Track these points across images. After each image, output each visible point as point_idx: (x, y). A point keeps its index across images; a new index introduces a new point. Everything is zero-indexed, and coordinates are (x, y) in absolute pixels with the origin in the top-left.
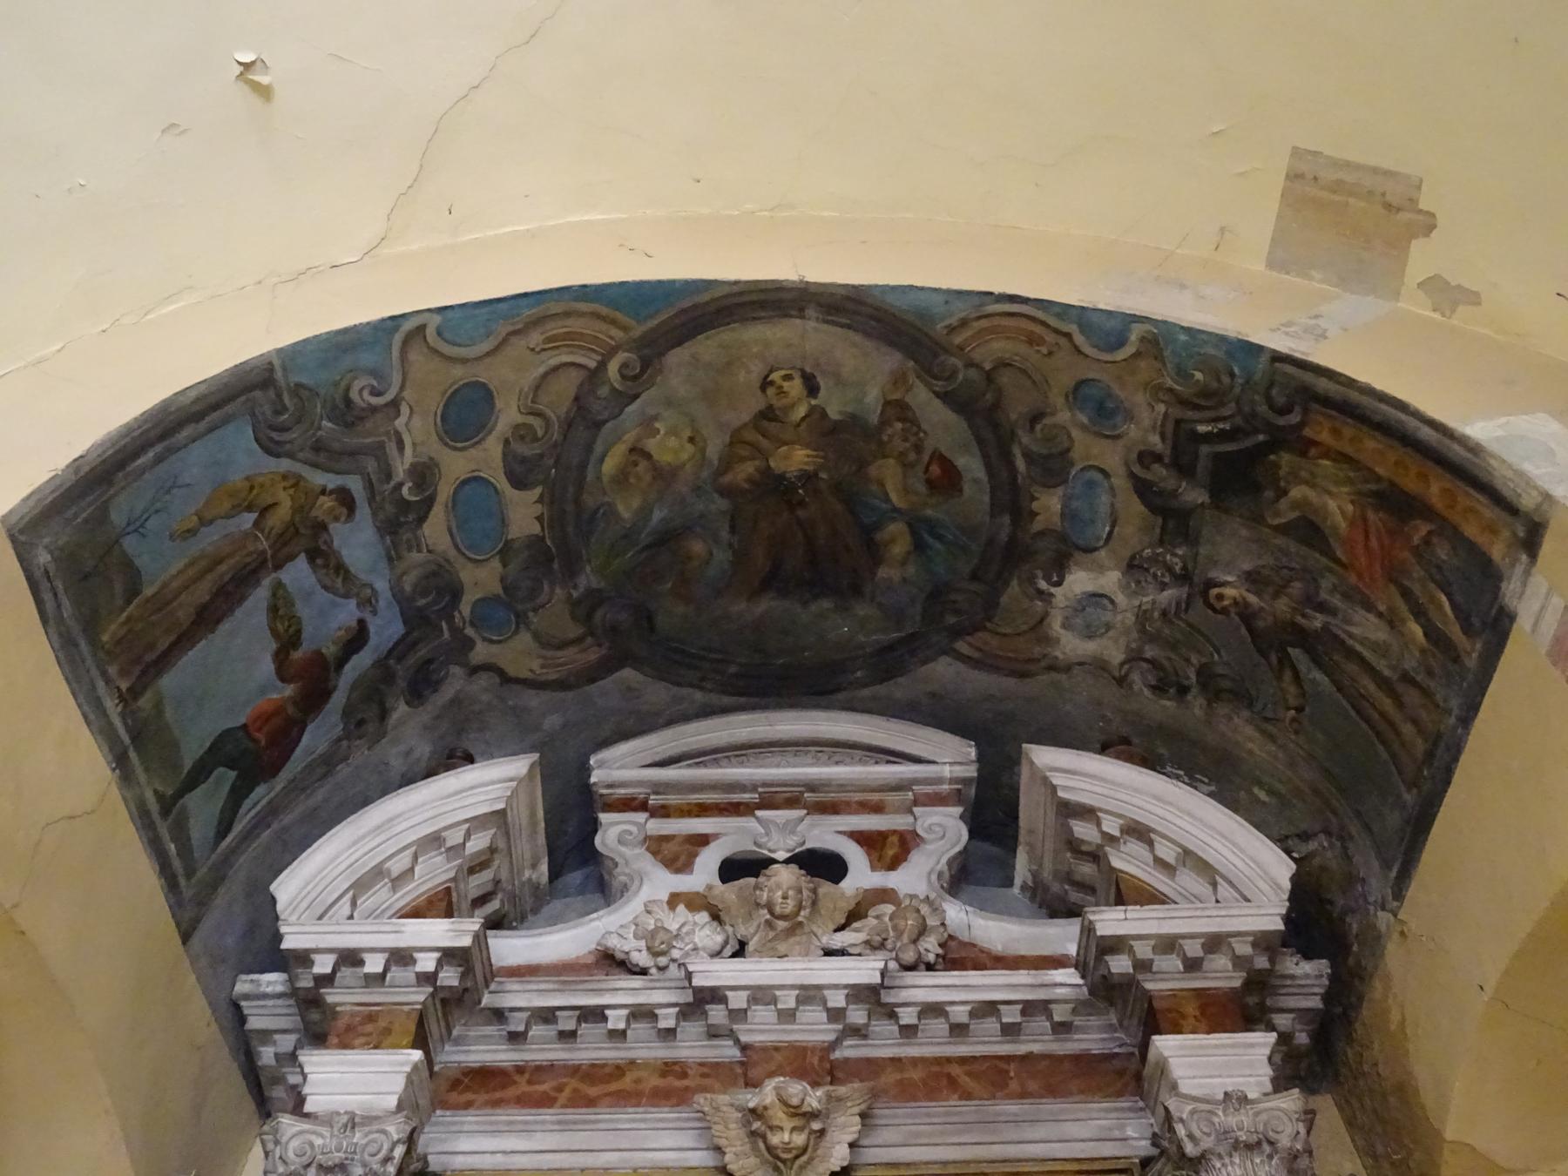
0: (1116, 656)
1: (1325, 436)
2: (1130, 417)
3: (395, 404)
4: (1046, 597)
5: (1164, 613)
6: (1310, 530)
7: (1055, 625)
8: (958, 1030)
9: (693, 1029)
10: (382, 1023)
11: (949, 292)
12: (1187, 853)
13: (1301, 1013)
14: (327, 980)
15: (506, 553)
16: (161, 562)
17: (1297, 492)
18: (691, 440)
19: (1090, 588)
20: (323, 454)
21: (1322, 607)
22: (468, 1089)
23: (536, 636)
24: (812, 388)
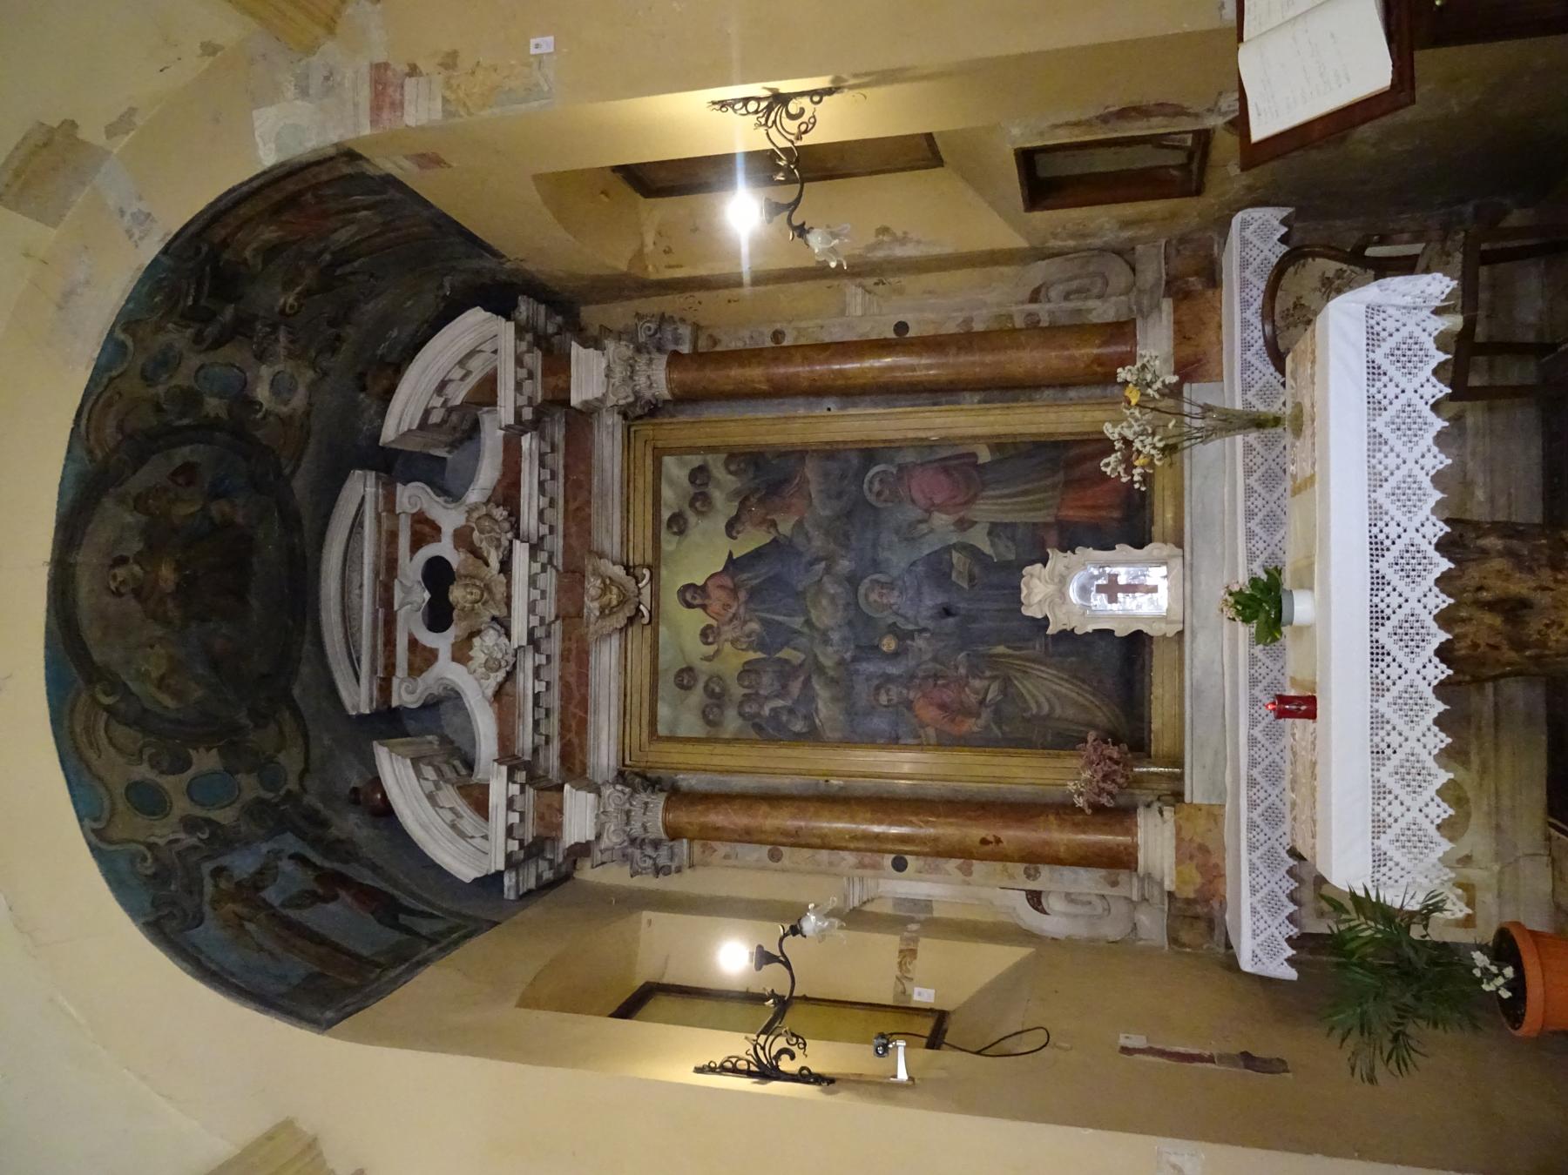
0: (310, 374)
1: (223, 233)
2: (170, 346)
3: (151, 846)
4: (268, 413)
5: (292, 342)
6: (271, 252)
7: (284, 410)
8: (552, 503)
9: (544, 646)
11: (67, 459)
13: (548, 317)
14: (521, 842)
15: (231, 771)
16: (298, 967)
17: (248, 254)
18: (152, 647)
19: (267, 387)
20: (193, 887)
21: (321, 253)
23: (278, 751)
24: (122, 561)
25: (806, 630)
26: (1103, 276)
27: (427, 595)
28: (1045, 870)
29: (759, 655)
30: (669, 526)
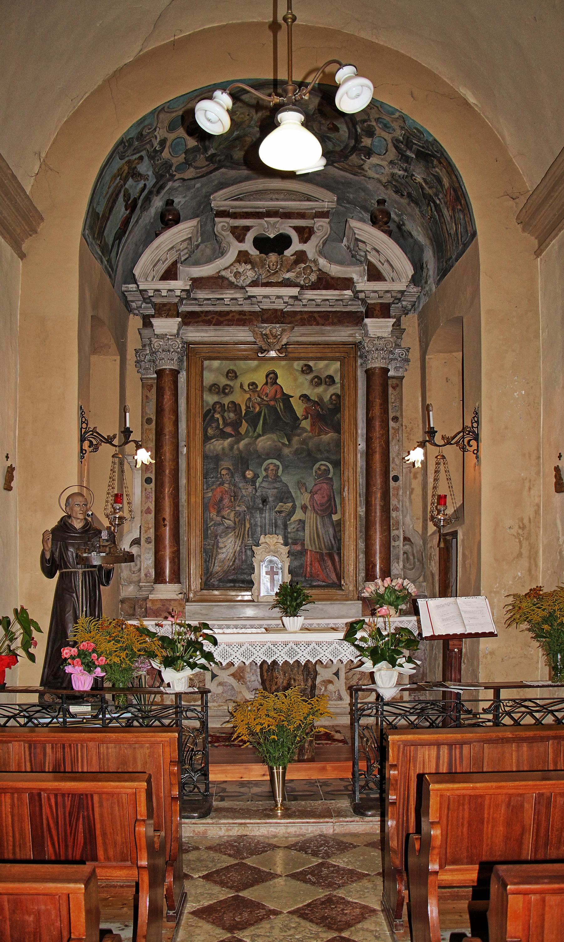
0: (384, 180)
10: (168, 307)
12: (388, 261)
22: (189, 318)
25: (256, 434)
26: (413, 569)
27: (272, 236)
28: (152, 546)
29: (244, 412)
30: (306, 365)
